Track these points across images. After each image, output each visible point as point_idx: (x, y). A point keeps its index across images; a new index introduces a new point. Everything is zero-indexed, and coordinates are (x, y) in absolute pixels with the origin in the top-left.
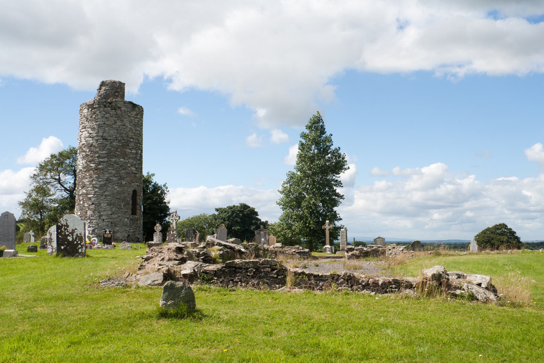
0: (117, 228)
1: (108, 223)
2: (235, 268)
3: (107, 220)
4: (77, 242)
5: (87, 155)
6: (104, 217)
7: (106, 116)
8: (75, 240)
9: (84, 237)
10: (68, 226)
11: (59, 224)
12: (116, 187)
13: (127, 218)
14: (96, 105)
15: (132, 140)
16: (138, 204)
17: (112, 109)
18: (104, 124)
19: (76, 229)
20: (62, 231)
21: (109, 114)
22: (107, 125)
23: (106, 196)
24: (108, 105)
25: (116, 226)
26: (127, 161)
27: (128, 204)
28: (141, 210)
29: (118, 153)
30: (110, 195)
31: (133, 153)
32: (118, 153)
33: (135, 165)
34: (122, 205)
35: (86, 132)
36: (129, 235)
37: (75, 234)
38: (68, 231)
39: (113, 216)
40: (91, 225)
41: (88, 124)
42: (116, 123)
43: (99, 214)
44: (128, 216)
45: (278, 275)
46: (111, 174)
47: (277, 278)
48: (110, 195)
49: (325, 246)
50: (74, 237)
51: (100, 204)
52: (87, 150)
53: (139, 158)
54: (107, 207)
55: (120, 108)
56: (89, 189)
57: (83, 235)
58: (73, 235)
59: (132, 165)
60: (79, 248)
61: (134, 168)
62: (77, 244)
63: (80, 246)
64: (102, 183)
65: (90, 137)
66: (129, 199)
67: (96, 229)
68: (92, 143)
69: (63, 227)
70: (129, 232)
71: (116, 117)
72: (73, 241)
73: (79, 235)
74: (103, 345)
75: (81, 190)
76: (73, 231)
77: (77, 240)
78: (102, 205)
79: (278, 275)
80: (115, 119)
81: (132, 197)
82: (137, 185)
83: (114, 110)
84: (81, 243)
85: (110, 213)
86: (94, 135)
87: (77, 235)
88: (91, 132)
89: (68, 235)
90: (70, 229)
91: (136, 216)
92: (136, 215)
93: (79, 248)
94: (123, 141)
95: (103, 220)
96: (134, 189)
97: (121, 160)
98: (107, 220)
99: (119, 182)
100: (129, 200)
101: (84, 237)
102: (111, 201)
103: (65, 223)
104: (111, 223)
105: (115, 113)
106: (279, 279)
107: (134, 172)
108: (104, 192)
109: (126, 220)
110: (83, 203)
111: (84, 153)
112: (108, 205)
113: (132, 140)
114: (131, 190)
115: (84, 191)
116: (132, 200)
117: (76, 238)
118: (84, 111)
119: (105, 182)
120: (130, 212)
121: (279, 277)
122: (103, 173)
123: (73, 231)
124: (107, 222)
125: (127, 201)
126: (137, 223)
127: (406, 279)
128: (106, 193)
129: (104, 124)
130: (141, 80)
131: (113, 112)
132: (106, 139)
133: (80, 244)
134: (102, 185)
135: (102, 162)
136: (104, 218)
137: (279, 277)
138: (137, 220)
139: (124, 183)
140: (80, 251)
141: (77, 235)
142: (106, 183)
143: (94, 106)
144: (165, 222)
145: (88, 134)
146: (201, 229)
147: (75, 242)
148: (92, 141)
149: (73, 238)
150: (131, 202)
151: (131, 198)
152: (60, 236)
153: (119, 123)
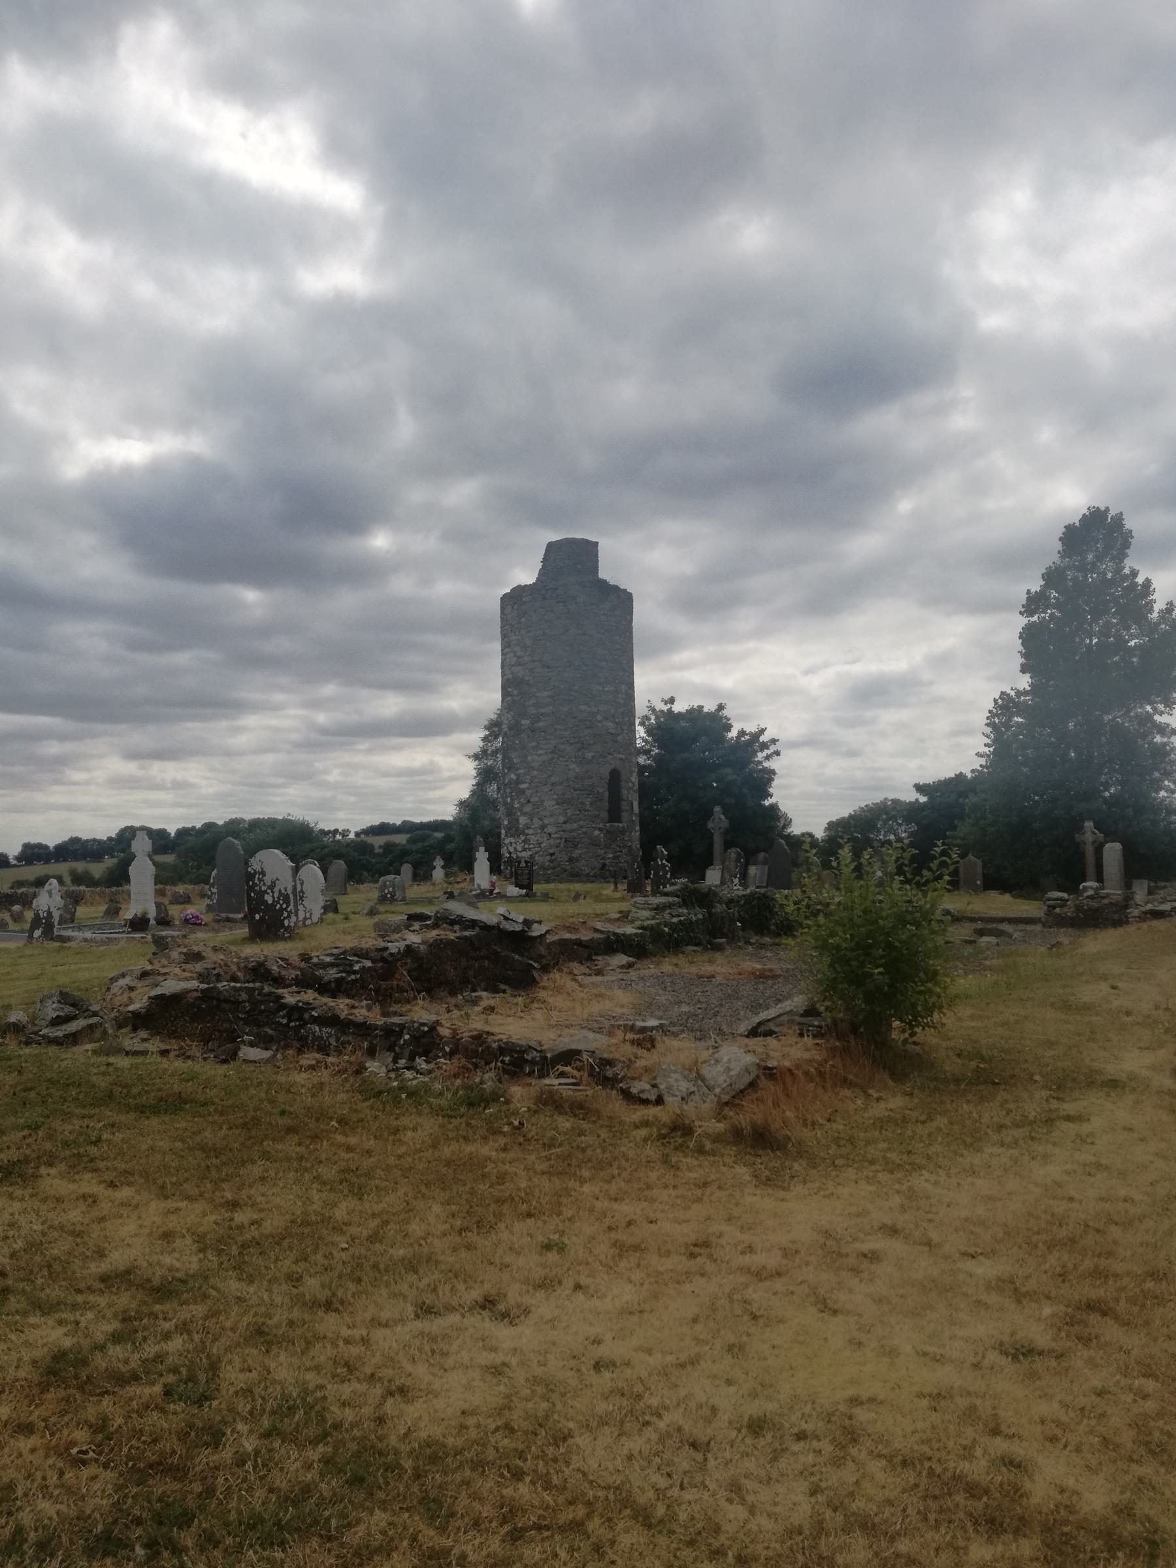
0: (578, 852)
1: (558, 841)
2: (218, 1000)
3: (556, 835)
4: (281, 906)
6: (550, 829)
8: (278, 902)
9: (291, 896)
10: (263, 873)
11: (250, 869)
12: (573, 766)
13: (600, 829)
15: (603, 664)
16: (624, 797)
18: (544, 634)
19: (277, 879)
20: (256, 885)
23: (553, 784)
25: (575, 846)
26: (596, 710)
27: (600, 800)
28: (632, 809)
29: (573, 694)
30: (561, 784)
31: (608, 691)
32: (573, 694)
33: (613, 716)
34: (588, 801)
35: (512, 655)
36: (604, 865)
37: (276, 890)
38: (264, 884)
39: (568, 826)
40: (526, 846)
42: (567, 630)
43: (541, 823)
44: (601, 825)
45: (290, 1021)
46: (562, 738)
47: (287, 1025)
48: (561, 784)
49: (1084, 884)
50: (276, 895)
51: (542, 801)
52: (515, 692)
53: (622, 701)
54: (557, 807)
56: (521, 771)
57: (290, 891)
58: (273, 892)
59: (606, 719)
60: (285, 918)
61: (611, 724)
62: (282, 910)
63: (285, 914)
64: (545, 758)
65: (519, 665)
66: (603, 790)
67: (536, 853)
69: (257, 876)
70: (603, 858)
72: (273, 905)
73: (283, 891)
76: (272, 887)
77: (281, 902)
78: (546, 804)
79: (290, 1021)
81: (609, 784)
82: (621, 759)
84: (287, 907)
85: (562, 819)
86: (527, 659)
87: (280, 891)
88: (519, 653)
89: (265, 892)
90: (268, 880)
91: (621, 825)
92: (620, 822)
93: (285, 918)
94: (585, 668)
95: (550, 835)
96: (613, 767)
97: (582, 707)
98: (556, 835)
99: (580, 753)
100: (601, 790)
101: (291, 896)
102: (563, 794)
103: (258, 868)
104: (566, 841)
106: (293, 1027)
107: (611, 731)
108: (549, 776)
109: (597, 833)
110: (512, 800)
111: (510, 698)
112: (558, 804)
113: (603, 664)
114: (605, 771)
115: (513, 776)
116: (609, 791)
117: (279, 898)
119: (550, 756)
120: (605, 815)
121: (292, 1024)
122: (545, 739)
123: (272, 887)
124: (557, 838)
125: (598, 793)
126: (623, 839)
128: (553, 779)
129: (544, 634)
130: (592, 539)
132: (548, 667)
133: (286, 909)
134: (544, 762)
135: (542, 714)
136: (551, 830)
137: (292, 1024)
138: (623, 832)
139: (589, 755)
140: (286, 923)
141: (280, 891)
142: (552, 759)
147: (278, 906)
149: (273, 896)
150: (606, 794)
151: (606, 786)
152: (252, 894)
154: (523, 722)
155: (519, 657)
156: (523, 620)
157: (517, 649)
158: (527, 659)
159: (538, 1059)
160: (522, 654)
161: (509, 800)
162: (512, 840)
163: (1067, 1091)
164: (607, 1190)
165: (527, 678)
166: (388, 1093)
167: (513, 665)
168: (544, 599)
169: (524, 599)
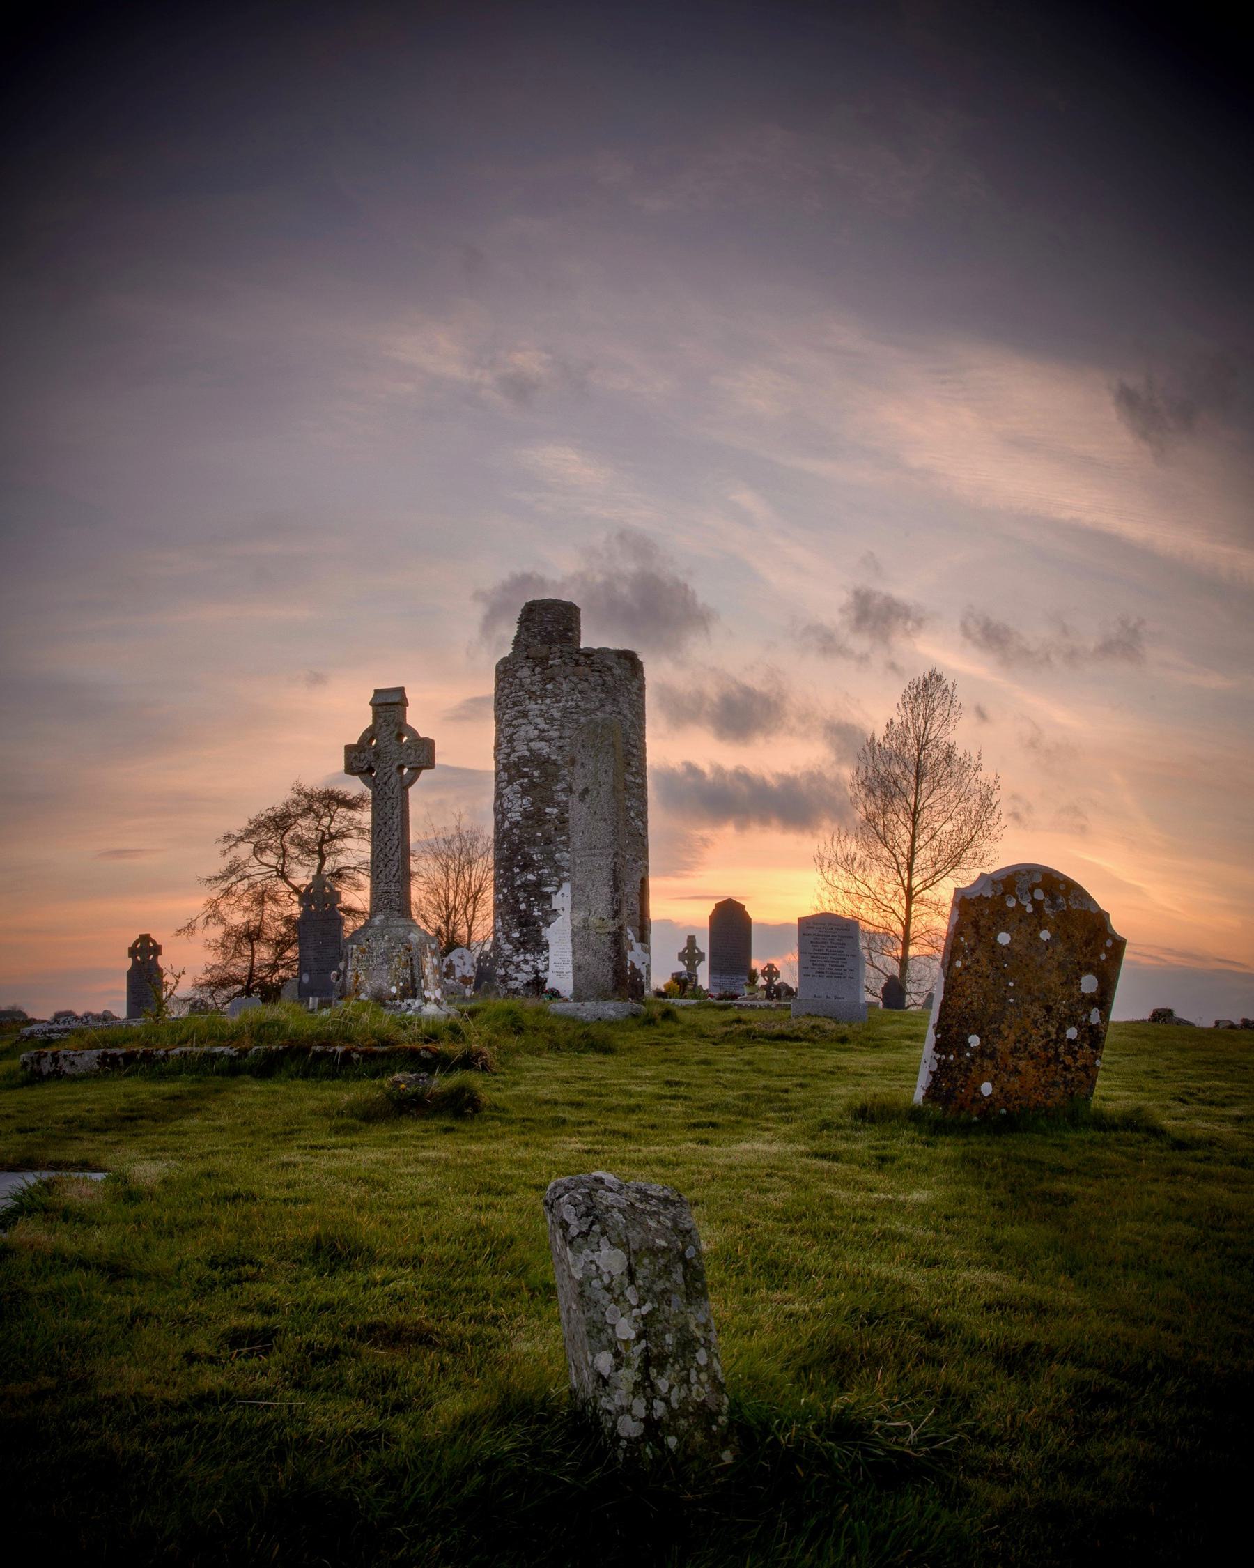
5: (534, 785)
7: (579, 686)
14: (554, 659)
17: (593, 671)
21: (586, 684)
22: (585, 710)
24: (582, 659)
41: (535, 706)
55: (610, 668)
65: (542, 740)
68: (548, 755)
71: (603, 692)
74: (640, 1282)
75: (518, 873)
80: (600, 695)
83: (597, 674)
105: (600, 682)
110: (529, 906)
115: (531, 877)
118: (518, 674)
127: (852, 785)
129: (577, 706)
131: (594, 678)
143: (551, 662)
144: (661, 1435)
145: (536, 732)
146: (727, 1258)
148: (548, 750)
153: (608, 708)
154: (548, 810)
155: (542, 731)
156: (549, 686)
157: (540, 721)
158: (554, 734)
159: (283, 930)
160: (547, 727)
161: (523, 906)
162: (529, 957)
163: (910, 624)
164: (669, 1330)
165: (553, 757)
166: (961, 934)
167: (532, 740)
168: (577, 664)
169: (551, 662)
